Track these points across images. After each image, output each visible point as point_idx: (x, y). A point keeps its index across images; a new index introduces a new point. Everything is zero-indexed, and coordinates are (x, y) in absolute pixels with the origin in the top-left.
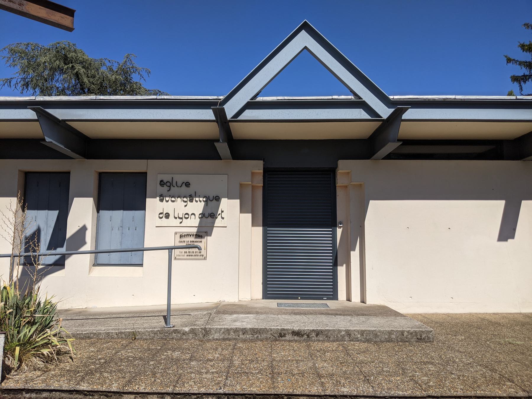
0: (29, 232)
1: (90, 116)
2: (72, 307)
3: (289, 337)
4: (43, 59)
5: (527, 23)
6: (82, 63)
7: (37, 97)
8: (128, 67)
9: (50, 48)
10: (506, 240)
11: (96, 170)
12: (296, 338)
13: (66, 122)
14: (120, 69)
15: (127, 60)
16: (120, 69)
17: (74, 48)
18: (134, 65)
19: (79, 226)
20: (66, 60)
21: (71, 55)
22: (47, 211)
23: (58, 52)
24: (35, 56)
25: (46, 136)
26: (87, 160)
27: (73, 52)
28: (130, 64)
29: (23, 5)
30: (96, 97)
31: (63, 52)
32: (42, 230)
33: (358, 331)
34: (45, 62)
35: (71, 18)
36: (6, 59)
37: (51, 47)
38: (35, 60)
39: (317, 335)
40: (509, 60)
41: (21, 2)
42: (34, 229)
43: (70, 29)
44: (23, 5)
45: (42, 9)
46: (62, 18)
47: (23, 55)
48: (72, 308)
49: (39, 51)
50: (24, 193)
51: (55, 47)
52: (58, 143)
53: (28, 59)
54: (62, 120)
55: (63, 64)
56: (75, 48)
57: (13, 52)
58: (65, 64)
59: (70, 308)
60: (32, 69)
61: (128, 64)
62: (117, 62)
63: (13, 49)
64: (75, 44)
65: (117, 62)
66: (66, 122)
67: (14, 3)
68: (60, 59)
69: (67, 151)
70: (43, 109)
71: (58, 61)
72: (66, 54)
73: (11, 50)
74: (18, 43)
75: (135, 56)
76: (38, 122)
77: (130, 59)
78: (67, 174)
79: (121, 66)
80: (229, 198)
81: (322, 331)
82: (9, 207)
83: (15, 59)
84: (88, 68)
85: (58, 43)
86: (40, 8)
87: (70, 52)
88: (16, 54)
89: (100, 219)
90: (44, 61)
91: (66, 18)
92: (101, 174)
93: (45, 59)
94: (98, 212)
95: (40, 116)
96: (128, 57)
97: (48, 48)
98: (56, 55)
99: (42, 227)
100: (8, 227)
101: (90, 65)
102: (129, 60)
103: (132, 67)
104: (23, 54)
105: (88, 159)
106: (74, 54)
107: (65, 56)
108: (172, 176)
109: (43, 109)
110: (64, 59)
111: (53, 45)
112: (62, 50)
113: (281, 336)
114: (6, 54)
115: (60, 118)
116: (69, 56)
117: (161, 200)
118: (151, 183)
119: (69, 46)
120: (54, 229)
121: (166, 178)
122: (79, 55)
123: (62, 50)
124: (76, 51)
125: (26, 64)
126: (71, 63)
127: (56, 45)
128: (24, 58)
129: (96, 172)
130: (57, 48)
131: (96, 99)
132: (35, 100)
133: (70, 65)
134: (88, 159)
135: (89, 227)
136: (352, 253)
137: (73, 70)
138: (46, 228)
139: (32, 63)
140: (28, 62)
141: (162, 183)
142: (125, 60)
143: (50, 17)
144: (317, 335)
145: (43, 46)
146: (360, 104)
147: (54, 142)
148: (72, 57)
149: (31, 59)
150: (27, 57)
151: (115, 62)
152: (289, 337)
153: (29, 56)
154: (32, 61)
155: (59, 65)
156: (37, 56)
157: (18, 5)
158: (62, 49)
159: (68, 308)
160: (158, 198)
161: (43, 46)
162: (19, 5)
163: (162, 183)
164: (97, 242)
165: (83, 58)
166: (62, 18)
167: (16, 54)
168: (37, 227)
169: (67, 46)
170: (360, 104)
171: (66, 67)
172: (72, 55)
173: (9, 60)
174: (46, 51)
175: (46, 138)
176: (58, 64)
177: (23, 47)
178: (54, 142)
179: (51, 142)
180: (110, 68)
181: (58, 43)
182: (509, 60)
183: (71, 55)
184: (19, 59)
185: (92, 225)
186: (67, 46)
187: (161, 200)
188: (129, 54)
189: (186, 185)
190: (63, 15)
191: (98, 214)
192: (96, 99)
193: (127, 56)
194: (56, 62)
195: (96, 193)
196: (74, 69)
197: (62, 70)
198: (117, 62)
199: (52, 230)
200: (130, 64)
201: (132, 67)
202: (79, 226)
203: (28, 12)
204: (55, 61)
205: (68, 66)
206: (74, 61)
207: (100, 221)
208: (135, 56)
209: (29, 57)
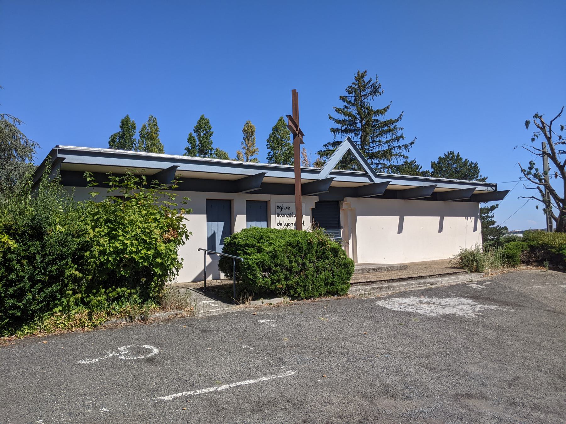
3: (371, 271)
5: (413, 145)
10: (400, 233)
12: (373, 271)
33: (389, 267)
39: (379, 269)
40: (330, 118)
78: (229, 202)
80: (306, 215)
81: (380, 268)
99: (216, 232)
108: (282, 203)
113: (369, 271)
117: (278, 216)
118: (272, 207)
121: (280, 205)
136: (349, 240)
141: (278, 207)
144: (379, 269)
146: (367, 176)
152: (371, 271)
160: (276, 215)
163: (278, 207)
170: (367, 176)
182: (330, 118)
187: (278, 216)
189: (288, 209)
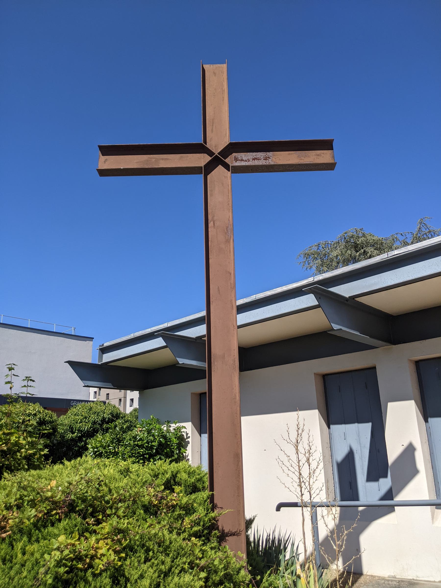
0: (340, 456)
1: (385, 282)
2: (418, 577)
4: (335, 253)
6: (373, 245)
7: (315, 277)
8: (424, 233)
9: (339, 241)
11: (410, 359)
13: (355, 299)
14: (415, 238)
15: (421, 226)
16: (415, 238)
17: (362, 232)
18: (431, 229)
19: (403, 445)
20: (356, 247)
21: (360, 241)
22: (356, 424)
23: (347, 242)
24: (326, 253)
25: (332, 323)
26: (394, 346)
27: (362, 237)
28: (426, 229)
29: (269, 158)
30: (388, 254)
31: (352, 240)
32: (355, 452)
34: (337, 256)
35: (330, 152)
36: (302, 264)
37: (339, 239)
38: (328, 257)
41: (267, 156)
42: (346, 451)
43: (330, 167)
44: (269, 158)
45: (292, 154)
46: (318, 155)
47: (316, 256)
48: (418, 579)
49: (330, 248)
50: (326, 403)
51: (343, 238)
52: (349, 329)
53: (321, 258)
54: (349, 297)
55: (354, 252)
56: (363, 232)
57: (307, 255)
58: (357, 251)
59: (415, 578)
60: (326, 266)
61: (423, 229)
62: (411, 233)
63: (306, 253)
64: (362, 228)
65: (411, 233)
66: (355, 299)
67: (259, 159)
68: (351, 248)
69: (366, 339)
70: (327, 289)
71: (349, 250)
72: (356, 241)
73: (305, 255)
74: (310, 247)
75: (429, 218)
76: (321, 308)
77: (424, 224)
79: (416, 234)
82: (286, 437)
83: (309, 261)
84: (380, 248)
85: (346, 233)
86: (289, 154)
87: (359, 238)
88: (310, 257)
89: (432, 432)
90: (336, 255)
91: (323, 153)
92: (418, 363)
93: (336, 252)
94: (426, 421)
95: (320, 298)
96: (421, 223)
97: (337, 241)
98: (346, 246)
100: (289, 470)
101: (382, 245)
102: (424, 225)
103: (430, 232)
104: (316, 255)
105: (395, 345)
106: (363, 238)
107: (355, 243)
109: (327, 289)
110: (354, 248)
111: (341, 237)
112: (351, 238)
114: (302, 259)
115: (347, 295)
116: (359, 243)
119: (357, 232)
120: (370, 450)
122: (369, 238)
123: (351, 238)
124: (364, 235)
125: (320, 263)
126: (362, 249)
127: (344, 235)
128: (317, 258)
129: (411, 361)
130: (345, 238)
131: (388, 257)
132: (313, 280)
133: (362, 251)
134: (395, 344)
135: (418, 445)
137: (365, 255)
138: (359, 447)
139: (325, 261)
140: (321, 261)
142: (419, 227)
143: (303, 160)
145: (333, 241)
147: (344, 328)
148: (362, 243)
149: (324, 257)
150: (320, 256)
151: (408, 233)
153: (321, 255)
154: (325, 259)
155: (351, 254)
156: (329, 253)
157: (264, 160)
158: (350, 237)
159: (411, 578)
161: (333, 241)
162: (265, 160)
164: (434, 469)
165: (374, 239)
166: (318, 155)
167: (310, 257)
168: (349, 448)
169: (355, 234)
171: (358, 253)
172: (362, 240)
173: (305, 264)
174: (335, 245)
175: (333, 325)
176: (349, 253)
177: (315, 249)
178: (344, 328)
179: (341, 329)
180: (403, 242)
181: (346, 233)
183: (360, 240)
184: (313, 261)
185: (421, 442)
186: (355, 234)
188: (422, 218)
190: (319, 152)
191: (427, 424)
192: (388, 257)
193: (421, 222)
194: (347, 252)
195: (417, 392)
196: (367, 254)
197: (355, 258)
198: (410, 233)
199: (368, 451)
200: (426, 229)
201: (430, 232)
202: (403, 445)
203: (276, 164)
204: (346, 252)
205: (360, 252)
206: (364, 246)
207: (432, 435)
208: (429, 218)
209: (321, 256)
